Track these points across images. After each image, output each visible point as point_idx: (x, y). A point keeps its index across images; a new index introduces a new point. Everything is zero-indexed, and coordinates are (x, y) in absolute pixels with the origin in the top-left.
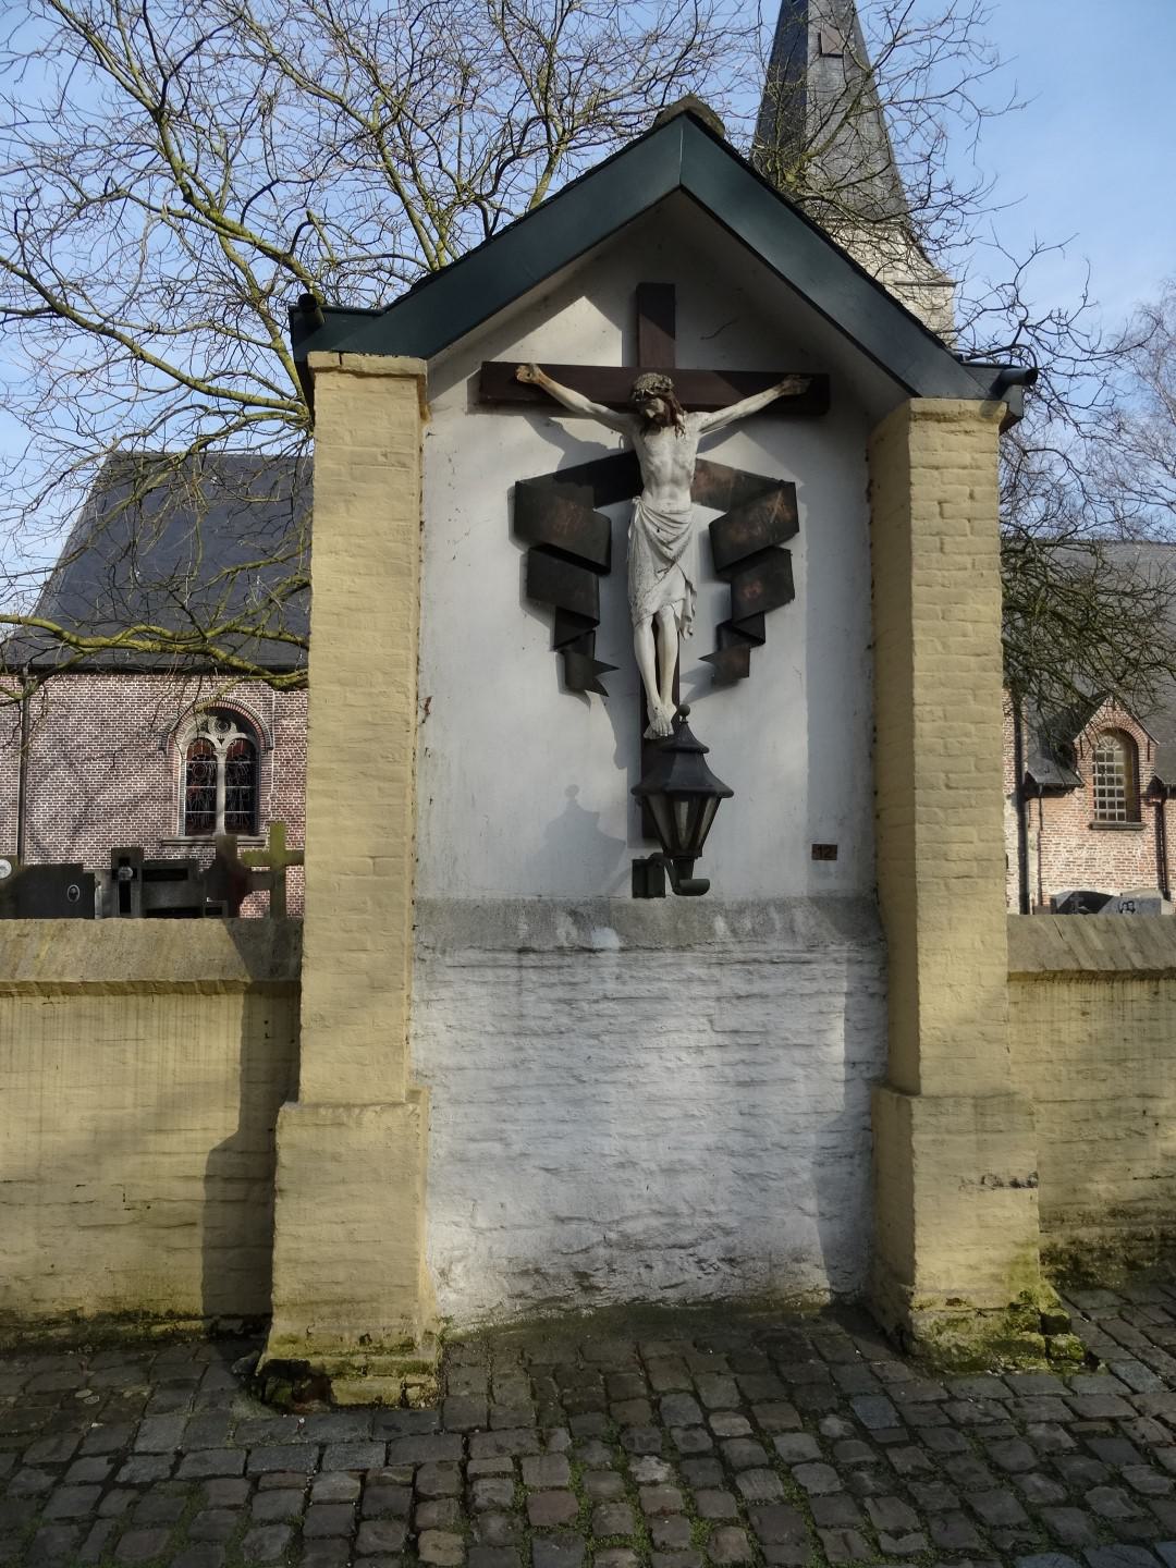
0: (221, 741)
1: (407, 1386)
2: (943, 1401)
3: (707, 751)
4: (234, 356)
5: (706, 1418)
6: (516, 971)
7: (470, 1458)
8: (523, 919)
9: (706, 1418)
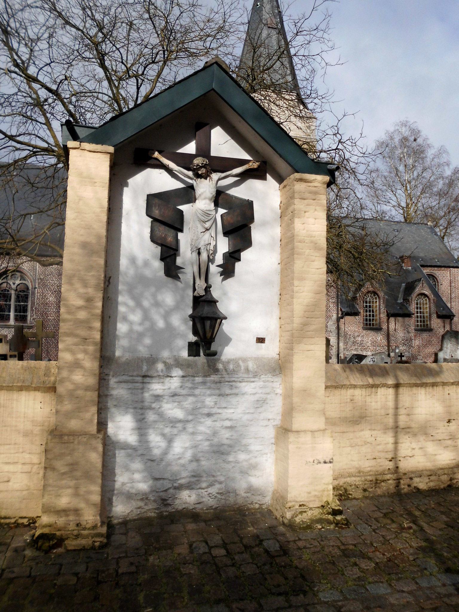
0: (14, 284)
1: (94, 542)
2: (296, 541)
3: (218, 302)
4: (30, 127)
5: (210, 550)
6: (141, 384)
7: (119, 567)
8: (145, 364)
9: (210, 550)
